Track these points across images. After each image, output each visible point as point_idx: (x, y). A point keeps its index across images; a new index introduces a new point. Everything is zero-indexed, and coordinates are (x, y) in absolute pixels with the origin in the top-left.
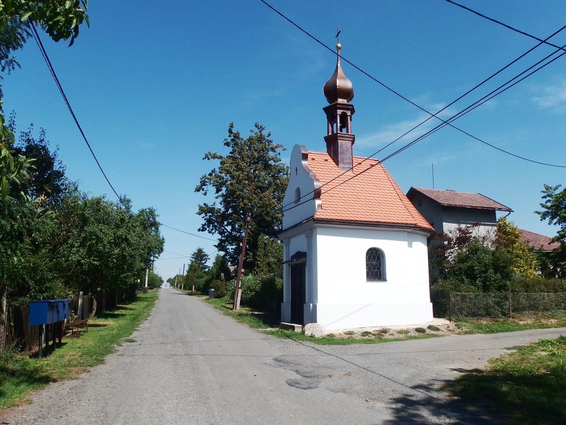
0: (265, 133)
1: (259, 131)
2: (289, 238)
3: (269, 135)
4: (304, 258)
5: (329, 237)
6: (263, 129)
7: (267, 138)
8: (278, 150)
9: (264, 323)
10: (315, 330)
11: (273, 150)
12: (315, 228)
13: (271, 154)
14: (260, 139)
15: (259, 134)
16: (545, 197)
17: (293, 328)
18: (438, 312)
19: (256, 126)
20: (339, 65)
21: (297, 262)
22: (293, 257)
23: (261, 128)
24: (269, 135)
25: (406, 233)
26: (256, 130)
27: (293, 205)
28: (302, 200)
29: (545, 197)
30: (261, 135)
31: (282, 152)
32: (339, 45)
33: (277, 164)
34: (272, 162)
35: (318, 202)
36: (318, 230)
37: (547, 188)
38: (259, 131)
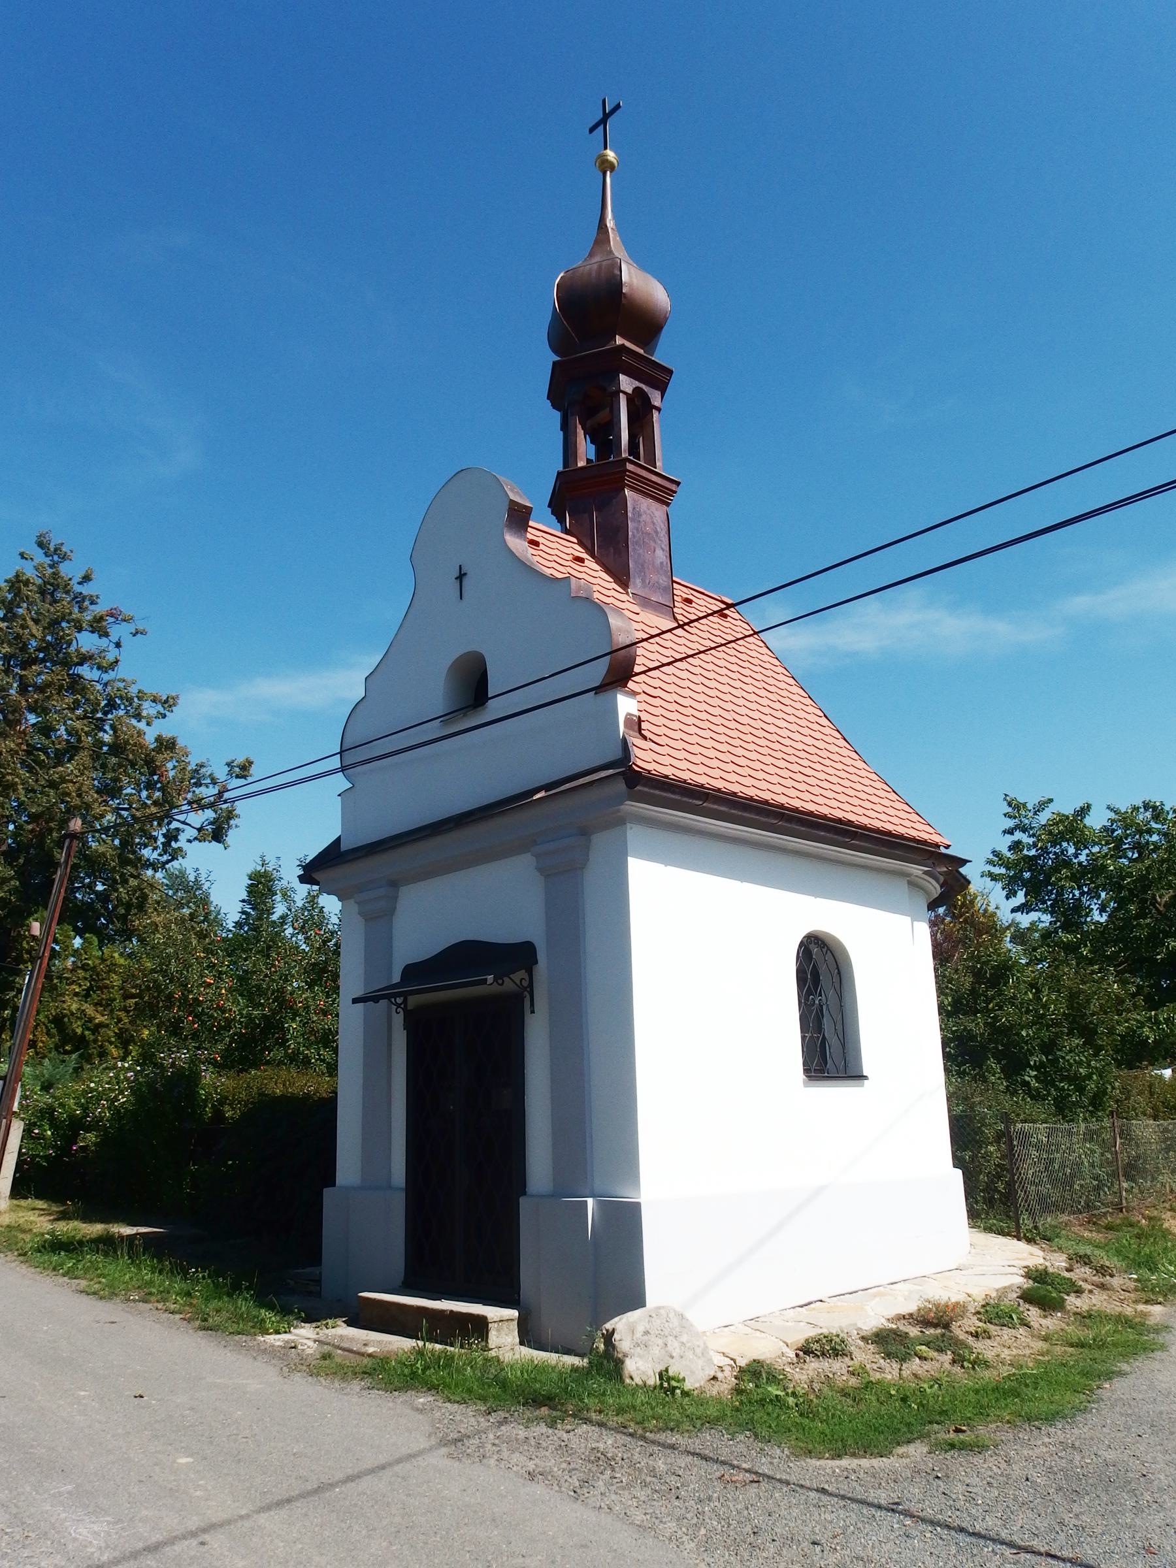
0: (70, 571)
1: (48, 561)
2: (394, 885)
3: (87, 578)
4: (522, 974)
5: (671, 870)
6: (64, 557)
7: (78, 589)
8: (117, 631)
9: (262, 1301)
10: (674, 1347)
11: (98, 627)
12: (621, 822)
13: (86, 642)
14: (52, 587)
15: (50, 571)
16: (1010, 832)
17: (480, 1326)
18: (995, 1199)
19: (41, 545)
20: (610, 223)
21: (496, 988)
22: (412, 972)
23: (57, 554)
24: (87, 578)
25: (903, 885)
26: (39, 556)
27: (434, 730)
28: (494, 708)
29: (1010, 832)
30: (56, 575)
31: (127, 641)
32: (611, 155)
33: (106, 677)
34: (87, 672)
35: (626, 705)
36: (634, 834)
37: (1016, 807)
38: (48, 561)
